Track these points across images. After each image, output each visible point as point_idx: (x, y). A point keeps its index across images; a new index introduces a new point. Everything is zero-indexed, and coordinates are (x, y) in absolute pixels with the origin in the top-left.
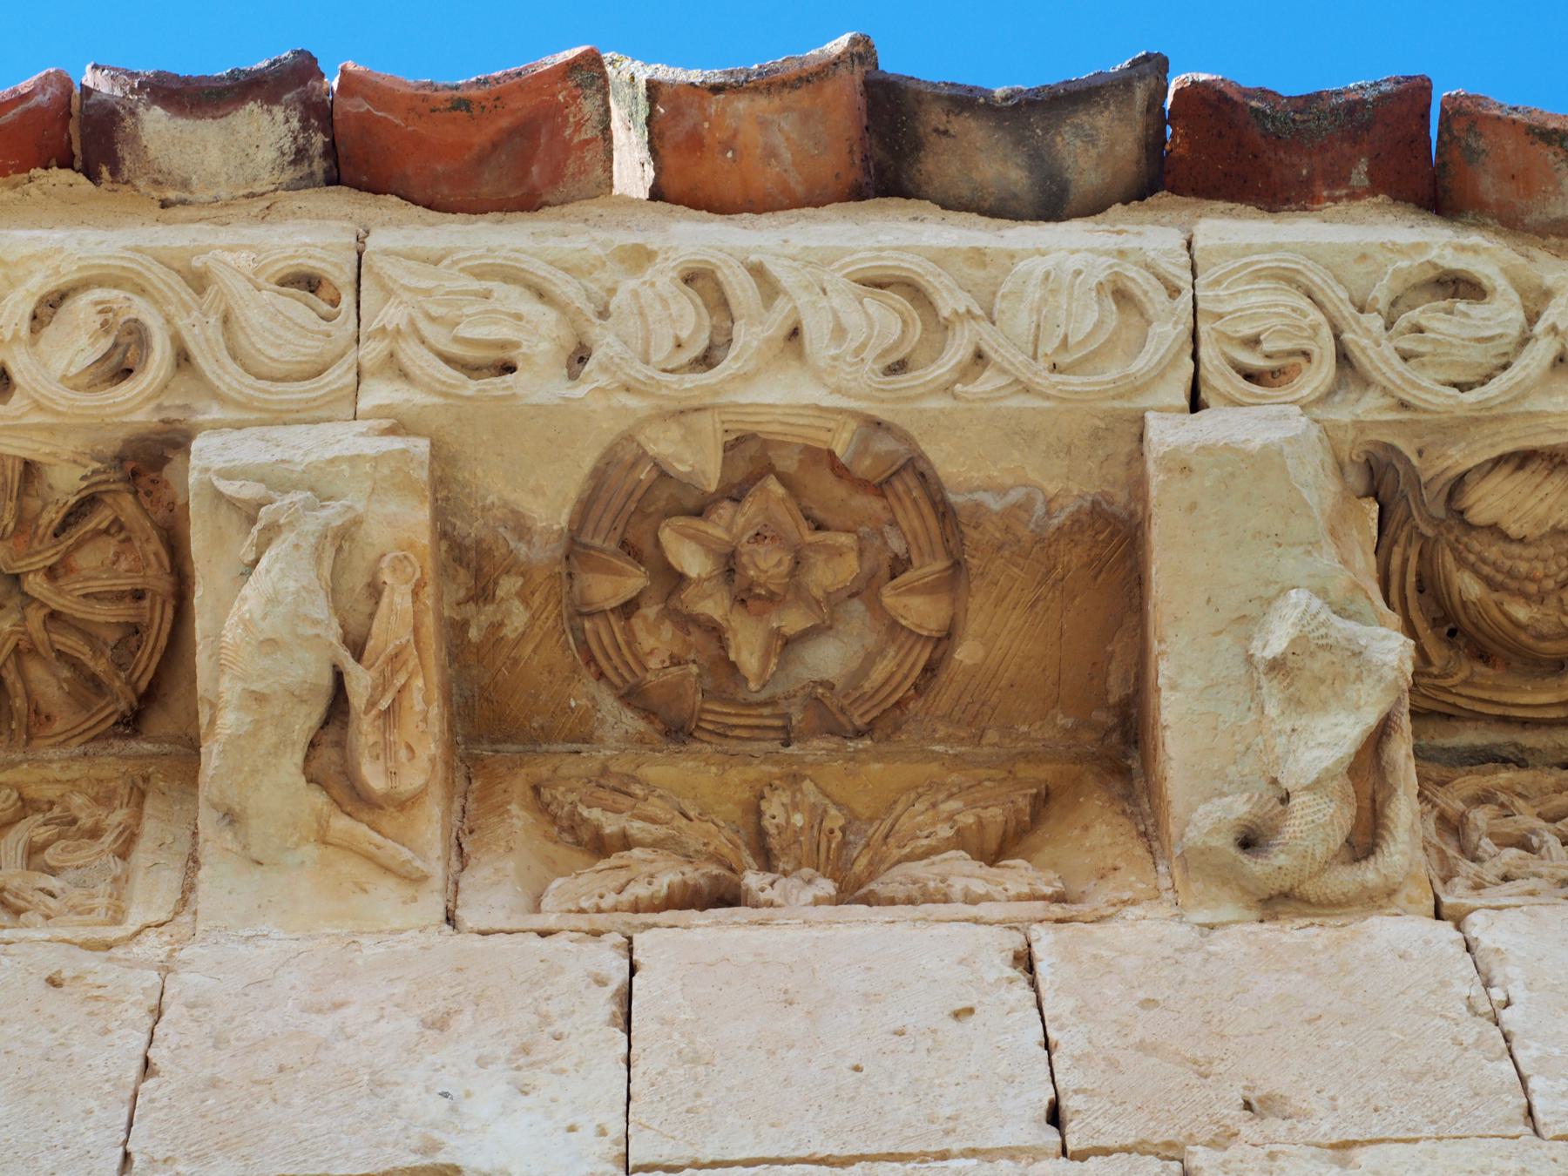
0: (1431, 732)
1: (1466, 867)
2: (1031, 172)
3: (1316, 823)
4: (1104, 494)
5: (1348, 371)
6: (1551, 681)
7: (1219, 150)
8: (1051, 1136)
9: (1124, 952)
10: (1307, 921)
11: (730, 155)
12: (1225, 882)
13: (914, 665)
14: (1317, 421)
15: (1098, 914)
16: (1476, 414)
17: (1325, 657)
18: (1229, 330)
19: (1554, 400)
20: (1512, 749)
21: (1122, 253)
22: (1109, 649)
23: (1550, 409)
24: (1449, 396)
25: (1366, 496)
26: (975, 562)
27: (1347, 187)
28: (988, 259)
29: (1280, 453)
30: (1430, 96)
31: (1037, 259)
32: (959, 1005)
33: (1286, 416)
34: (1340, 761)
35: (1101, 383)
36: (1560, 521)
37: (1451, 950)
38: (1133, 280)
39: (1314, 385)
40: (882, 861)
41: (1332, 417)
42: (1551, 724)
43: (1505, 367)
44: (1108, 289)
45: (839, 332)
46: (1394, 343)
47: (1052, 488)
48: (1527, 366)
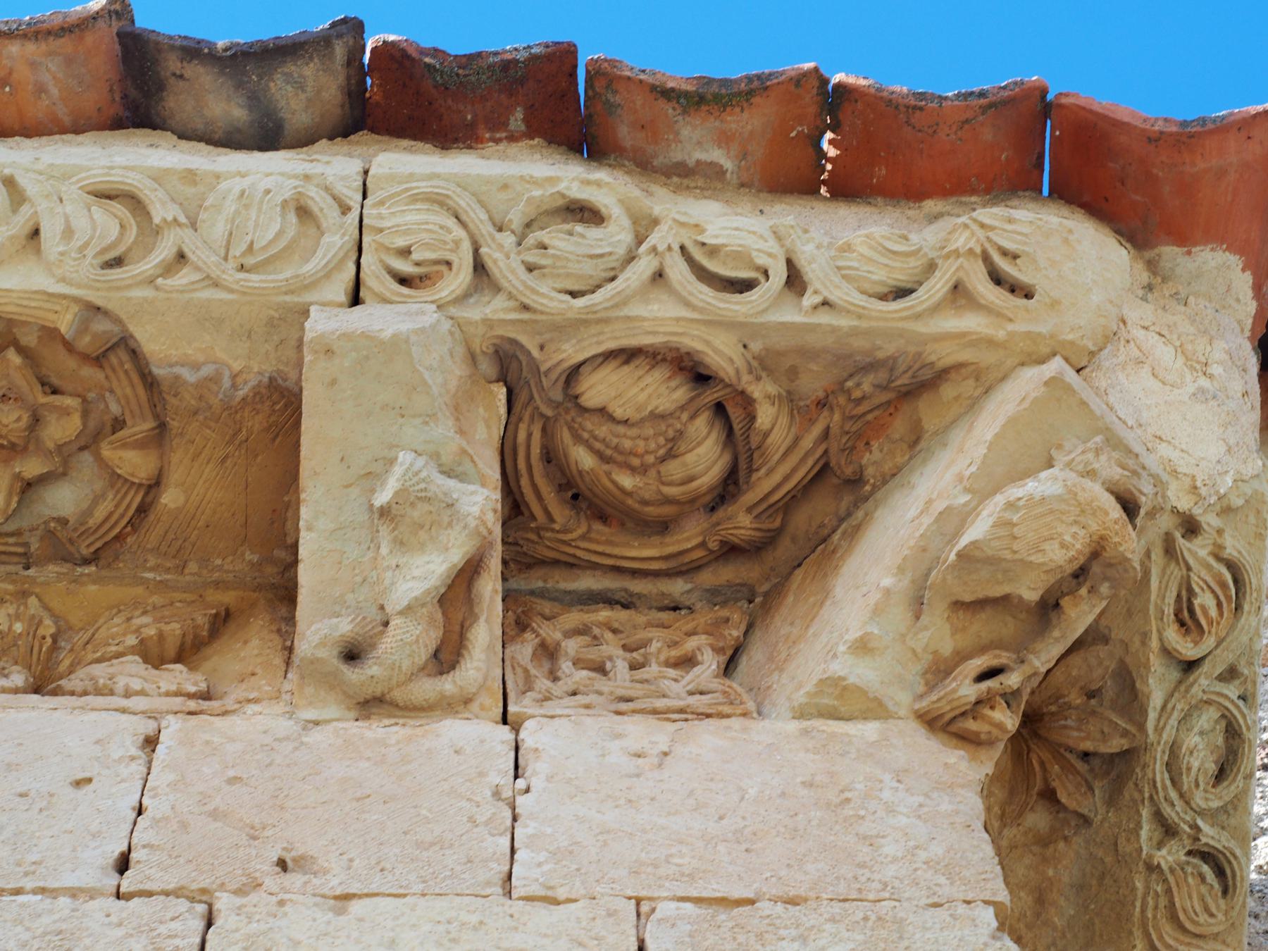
0: (557, 577)
1: (543, 683)
2: (251, 111)
3: (407, 642)
4: (279, 371)
5: (485, 278)
6: (656, 539)
7: (402, 98)
8: (112, 880)
9: (232, 740)
10: (393, 721)
11: (7, 89)
12: (332, 688)
13: (128, 507)
14: (452, 318)
15: (224, 709)
16: (584, 317)
17: (423, 507)
18: (387, 242)
19: (650, 307)
20: (623, 594)
21: (307, 177)
22: (286, 499)
23: (645, 314)
24: (562, 302)
25: (498, 381)
26: (175, 424)
27: (506, 131)
28: (198, 179)
29: (407, 341)
30: (576, 59)
31: (238, 179)
32: (80, 776)
33: (423, 313)
34: (428, 592)
35: (276, 281)
36: (657, 408)
37: (499, 748)
38: (312, 199)
39: (452, 288)
40: (79, 663)
41: (465, 315)
42: (656, 574)
43: (613, 279)
44: (292, 206)
45: (68, 232)
46: (522, 257)
47: (237, 366)
48: (628, 279)
